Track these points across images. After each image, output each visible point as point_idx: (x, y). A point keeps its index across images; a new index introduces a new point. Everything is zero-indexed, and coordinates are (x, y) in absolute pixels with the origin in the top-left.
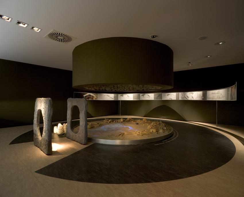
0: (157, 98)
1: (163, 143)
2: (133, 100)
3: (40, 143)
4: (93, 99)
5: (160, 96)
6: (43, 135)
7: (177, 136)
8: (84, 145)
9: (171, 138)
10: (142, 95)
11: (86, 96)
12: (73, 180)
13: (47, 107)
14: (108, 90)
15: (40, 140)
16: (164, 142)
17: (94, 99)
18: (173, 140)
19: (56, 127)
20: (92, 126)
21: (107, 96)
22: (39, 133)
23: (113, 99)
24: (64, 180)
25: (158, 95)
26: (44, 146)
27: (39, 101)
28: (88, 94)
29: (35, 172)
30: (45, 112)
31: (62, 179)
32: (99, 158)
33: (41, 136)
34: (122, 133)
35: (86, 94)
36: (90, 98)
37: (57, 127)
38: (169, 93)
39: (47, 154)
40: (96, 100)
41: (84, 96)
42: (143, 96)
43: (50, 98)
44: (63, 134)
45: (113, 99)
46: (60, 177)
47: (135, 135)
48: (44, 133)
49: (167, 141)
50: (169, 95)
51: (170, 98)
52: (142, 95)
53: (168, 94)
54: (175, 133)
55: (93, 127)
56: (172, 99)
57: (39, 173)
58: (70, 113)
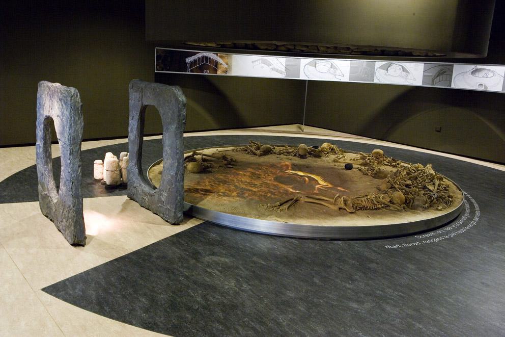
0: (433, 81)
1: (417, 244)
2: (348, 81)
3: (54, 211)
4: (216, 71)
5: (447, 74)
6: (60, 192)
7: (473, 223)
8: (174, 224)
9: (448, 228)
10: (381, 67)
11: (195, 61)
12: (132, 324)
13: (68, 113)
14: (262, 47)
15: (55, 201)
16: (420, 241)
17: (219, 73)
18: (452, 235)
19: (100, 161)
20: (206, 164)
21: (264, 62)
22: (51, 184)
23: (281, 72)
24: (110, 321)
25: (439, 68)
26: (64, 220)
27: (46, 93)
28: (201, 54)
29: (43, 290)
30: (64, 128)
31: (106, 318)
32: (209, 270)
33: (58, 192)
34: (291, 197)
35: (195, 54)
36: (208, 67)
37: (103, 161)
38: (479, 67)
39: (72, 242)
40: (225, 76)
41: (189, 60)
42: (386, 68)
43: (73, 90)
44: (119, 183)
45: (281, 72)
46: (101, 311)
47: (331, 207)
48: (62, 187)
49: (430, 238)
50: (477, 74)
51: (481, 85)
52: (381, 67)
53: (477, 70)
54: (468, 211)
55: (208, 167)
56: (486, 87)
57: (47, 292)
58: (136, 126)
